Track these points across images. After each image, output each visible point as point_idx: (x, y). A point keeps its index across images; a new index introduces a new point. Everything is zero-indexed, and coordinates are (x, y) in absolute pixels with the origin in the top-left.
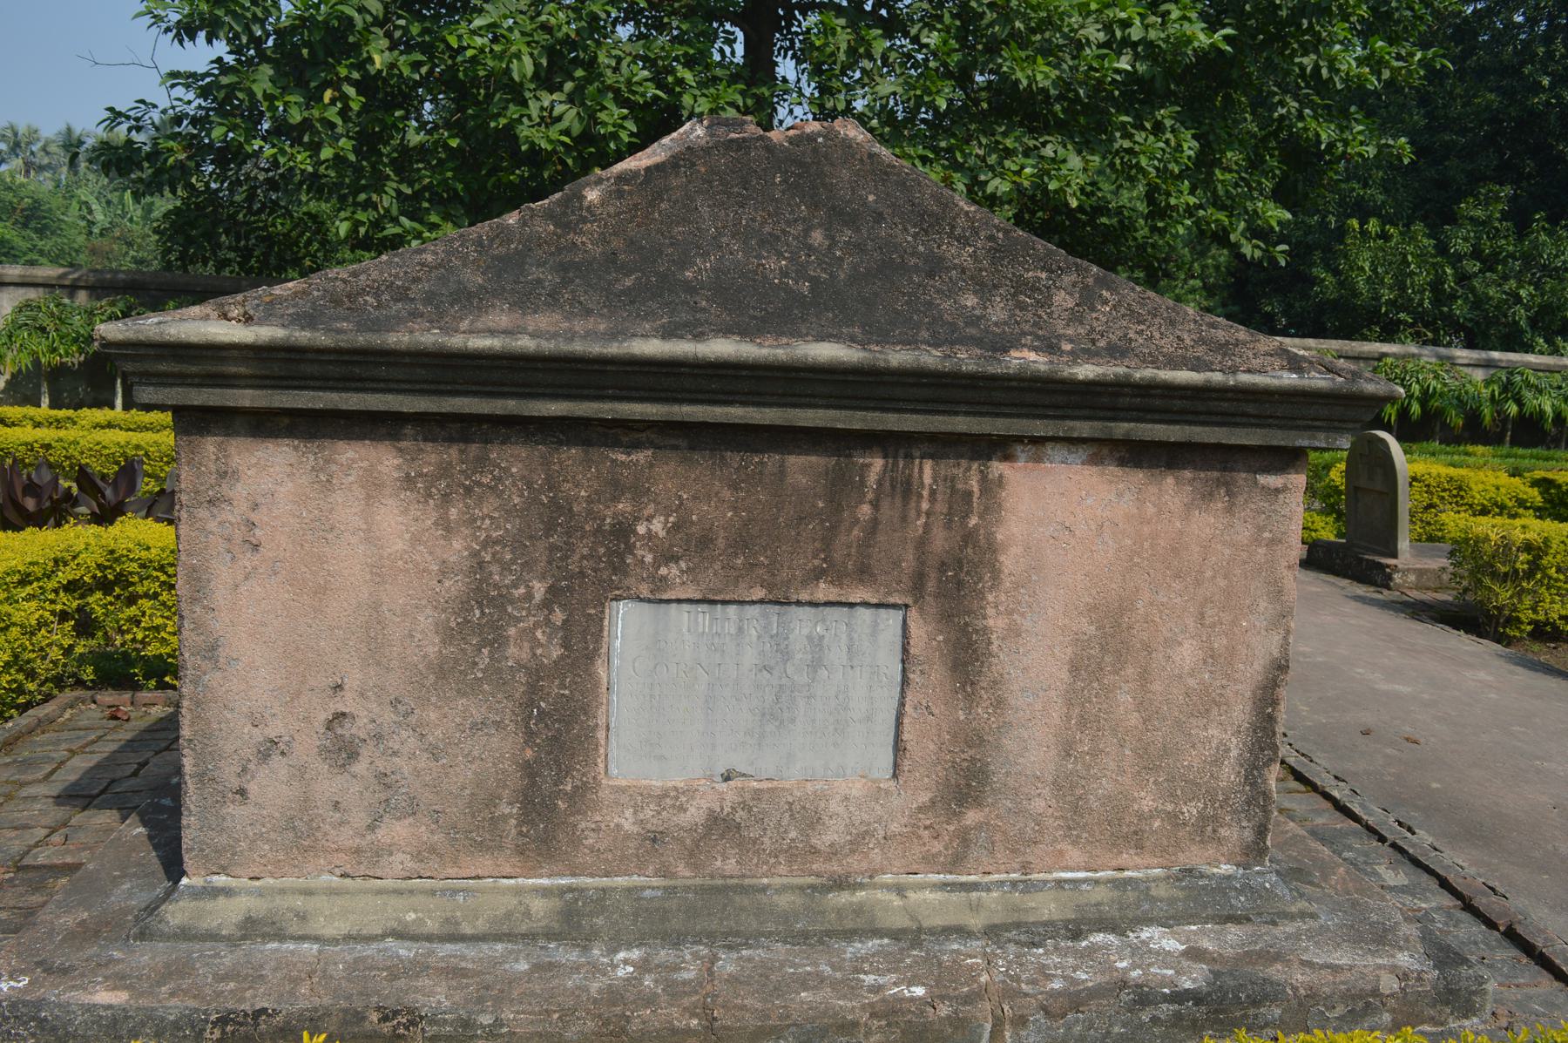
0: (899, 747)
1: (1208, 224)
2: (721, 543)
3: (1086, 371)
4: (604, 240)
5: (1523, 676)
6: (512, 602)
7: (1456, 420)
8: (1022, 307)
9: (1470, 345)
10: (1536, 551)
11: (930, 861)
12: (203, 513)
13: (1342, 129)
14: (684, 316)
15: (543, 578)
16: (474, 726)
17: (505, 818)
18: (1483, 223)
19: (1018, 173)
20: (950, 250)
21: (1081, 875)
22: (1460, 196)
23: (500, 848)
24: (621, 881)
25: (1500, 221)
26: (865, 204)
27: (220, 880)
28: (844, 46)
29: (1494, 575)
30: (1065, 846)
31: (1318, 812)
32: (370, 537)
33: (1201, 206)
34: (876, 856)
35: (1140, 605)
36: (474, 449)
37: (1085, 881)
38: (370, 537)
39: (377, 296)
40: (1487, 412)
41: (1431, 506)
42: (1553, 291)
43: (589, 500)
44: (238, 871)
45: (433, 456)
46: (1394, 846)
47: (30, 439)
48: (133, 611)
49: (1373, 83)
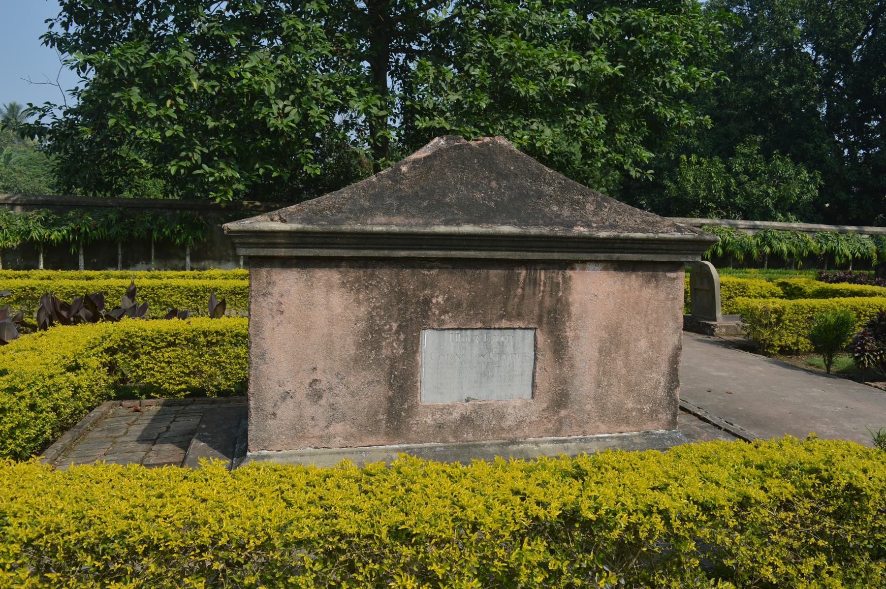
0: (534, 386)
1: (613, 161)
2: (465, 305)
3: (603, 234)
4: (411, 187)
5: (776, 368)
6: (384, 332)
7: (740, 256)
8: (575, 210)
9: (745, 218)
10: (779, 313)
11: (547, 431)
12: (260, 299)
13: (678, 111)
14: (450, 217)
15: (396, 321)
16: (369, 383)
17: (380, 420)
18: (749, 156)
19: (521, 139)
20: (545, 188)
21: (606, 435)
22: (737, 141)
23: (379, 433)
24: (427, 445)
25: (757, 154)
26: (510, 170)
27: (265, 452)
28: (432, 76)
29: (761, 325)
30: (599, 424)
31: (692, 421)
32: (328, 308)
33: (609, 152)
34: (526, 430)
35: (624, 325)
36: (369, 271)
37: (608, 437)
38: (328, 308)
39: (331, 211)
40: (755, 252)
41: (731, 297)
42: (784, 189)
43: (414, 290)
44: (271, 448)
45: (353, 274)
46: (725, 430)
47: (23, 285)
48: (137, 361)
49: (692, 90)
